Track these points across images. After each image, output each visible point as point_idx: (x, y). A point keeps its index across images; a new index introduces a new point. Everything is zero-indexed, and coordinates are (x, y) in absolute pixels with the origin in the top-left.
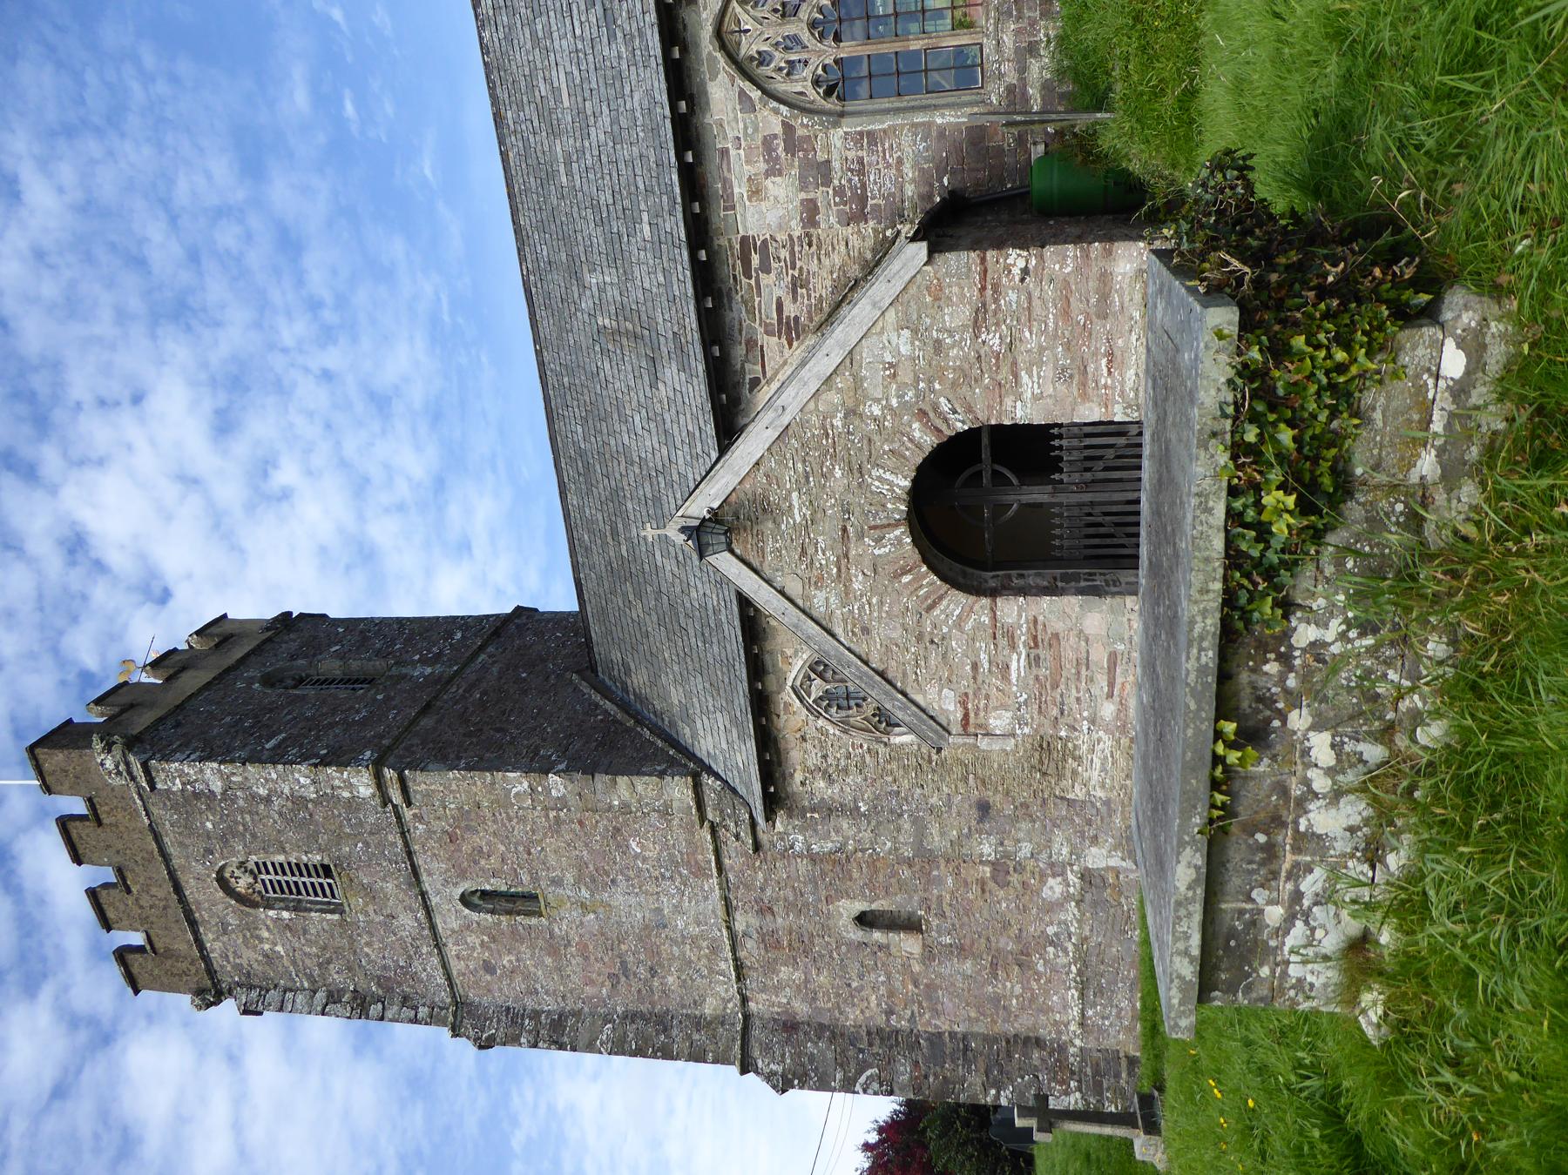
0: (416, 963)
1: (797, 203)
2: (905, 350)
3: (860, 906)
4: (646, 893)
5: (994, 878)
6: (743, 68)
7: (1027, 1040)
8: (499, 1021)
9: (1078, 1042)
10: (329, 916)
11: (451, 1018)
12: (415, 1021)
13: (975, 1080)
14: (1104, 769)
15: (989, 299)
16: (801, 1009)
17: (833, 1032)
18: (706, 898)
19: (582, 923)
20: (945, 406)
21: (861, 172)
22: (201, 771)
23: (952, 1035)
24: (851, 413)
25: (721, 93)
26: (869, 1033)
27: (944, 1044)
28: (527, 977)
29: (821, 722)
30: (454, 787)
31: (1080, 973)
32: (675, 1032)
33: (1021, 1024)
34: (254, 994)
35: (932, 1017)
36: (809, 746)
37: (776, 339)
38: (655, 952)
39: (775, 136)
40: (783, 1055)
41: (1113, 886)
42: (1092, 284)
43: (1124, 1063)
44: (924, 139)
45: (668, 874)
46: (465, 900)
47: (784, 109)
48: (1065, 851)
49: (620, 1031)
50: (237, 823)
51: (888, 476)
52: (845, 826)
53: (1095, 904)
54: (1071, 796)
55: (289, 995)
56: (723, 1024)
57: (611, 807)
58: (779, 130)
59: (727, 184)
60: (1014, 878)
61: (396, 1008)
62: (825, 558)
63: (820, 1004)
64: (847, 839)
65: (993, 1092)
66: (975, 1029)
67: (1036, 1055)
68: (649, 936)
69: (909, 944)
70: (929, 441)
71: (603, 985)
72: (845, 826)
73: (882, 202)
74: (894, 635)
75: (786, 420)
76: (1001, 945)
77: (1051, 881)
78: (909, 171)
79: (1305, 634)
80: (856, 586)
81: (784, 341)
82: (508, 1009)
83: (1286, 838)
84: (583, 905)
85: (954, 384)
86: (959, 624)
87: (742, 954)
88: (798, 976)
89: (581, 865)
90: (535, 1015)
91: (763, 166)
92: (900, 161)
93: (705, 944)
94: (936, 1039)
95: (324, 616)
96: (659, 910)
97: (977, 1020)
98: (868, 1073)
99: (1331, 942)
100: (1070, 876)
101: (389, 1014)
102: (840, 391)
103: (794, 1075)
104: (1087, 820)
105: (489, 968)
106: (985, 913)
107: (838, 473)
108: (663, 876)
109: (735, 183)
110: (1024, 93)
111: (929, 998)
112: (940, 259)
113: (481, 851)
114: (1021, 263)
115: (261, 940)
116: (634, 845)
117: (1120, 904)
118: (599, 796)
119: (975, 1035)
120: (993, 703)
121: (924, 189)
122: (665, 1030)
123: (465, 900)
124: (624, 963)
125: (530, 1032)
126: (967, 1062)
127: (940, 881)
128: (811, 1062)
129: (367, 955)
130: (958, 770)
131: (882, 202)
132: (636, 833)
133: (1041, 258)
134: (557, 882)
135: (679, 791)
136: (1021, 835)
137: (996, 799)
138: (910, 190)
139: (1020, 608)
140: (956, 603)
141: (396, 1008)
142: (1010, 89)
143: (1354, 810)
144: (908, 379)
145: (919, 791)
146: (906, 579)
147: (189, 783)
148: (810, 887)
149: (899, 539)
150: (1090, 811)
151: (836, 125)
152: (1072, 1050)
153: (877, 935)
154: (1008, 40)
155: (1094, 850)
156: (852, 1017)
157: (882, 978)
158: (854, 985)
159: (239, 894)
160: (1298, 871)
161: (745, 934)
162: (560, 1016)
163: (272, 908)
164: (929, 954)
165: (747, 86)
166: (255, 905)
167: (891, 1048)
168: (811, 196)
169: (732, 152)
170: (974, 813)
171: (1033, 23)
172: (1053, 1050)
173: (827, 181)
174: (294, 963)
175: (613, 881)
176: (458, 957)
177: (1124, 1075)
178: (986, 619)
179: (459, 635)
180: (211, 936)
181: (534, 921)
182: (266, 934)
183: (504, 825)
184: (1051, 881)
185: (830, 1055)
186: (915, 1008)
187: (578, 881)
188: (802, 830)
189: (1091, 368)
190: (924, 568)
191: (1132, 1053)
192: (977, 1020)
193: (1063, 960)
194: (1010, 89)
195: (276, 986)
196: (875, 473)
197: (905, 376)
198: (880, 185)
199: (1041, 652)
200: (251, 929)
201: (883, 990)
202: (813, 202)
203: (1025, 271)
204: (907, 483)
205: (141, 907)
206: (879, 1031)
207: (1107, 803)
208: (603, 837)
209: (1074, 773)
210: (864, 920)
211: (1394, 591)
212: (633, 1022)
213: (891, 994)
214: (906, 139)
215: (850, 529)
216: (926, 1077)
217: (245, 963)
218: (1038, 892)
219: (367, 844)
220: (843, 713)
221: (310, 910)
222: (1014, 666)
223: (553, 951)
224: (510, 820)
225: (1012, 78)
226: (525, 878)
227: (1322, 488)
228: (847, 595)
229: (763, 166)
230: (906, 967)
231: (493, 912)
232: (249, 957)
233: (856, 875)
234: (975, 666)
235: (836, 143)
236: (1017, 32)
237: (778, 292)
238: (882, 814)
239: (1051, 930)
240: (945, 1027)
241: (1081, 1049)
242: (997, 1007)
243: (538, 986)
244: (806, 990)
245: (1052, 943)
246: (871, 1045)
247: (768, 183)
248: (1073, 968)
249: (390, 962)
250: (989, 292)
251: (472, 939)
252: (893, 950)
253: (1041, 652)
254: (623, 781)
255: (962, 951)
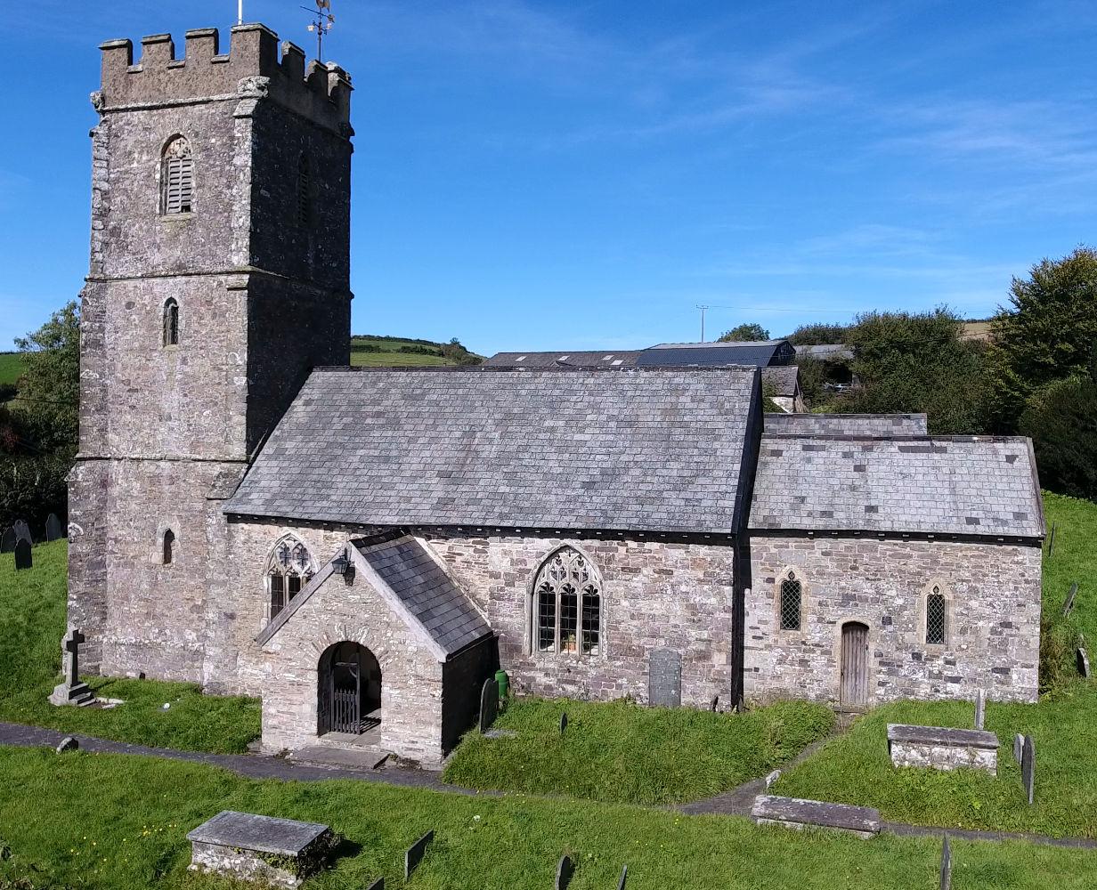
0: (130, 257)
3: (177, 534)
5: (195, 605)
6: (555, 554)
7: (105, 613)
8: (97, 307)
9: (105, 640)
10: (158, 206)
12: (93, 252)
13: (81, 587)
14: (252, 674)
16: (115, 491)
17: (102, 508)
18: (178, 448)
20: (389, 661)
21: (509, 600)
23: (105, 574)
25: (546, 545)
26: (103, 528)
27: (99, 569)
28: (126, 328)
30: (238, 319)
31: (145, 645)
32: (97, 416)
33: (112, 609)
34: (104, 139)
36: (262, 535)
37: (447, 550)
38: (145, 410)
40: (87, 481)
41: (193, 666)
42: (428, 720)
43: (96, 664)
44: (519, 628)
46: (171, 300)
47: (536, 570)
48: (211, 653)
49: (95, 383)
50: (215, 160)
51: (364, 636)
53: (183, 656)
55: (105, 164)
57: (229, 410)
58: (528, 567)
60: (195, 616)
61: (101, 238)
62: (335, 605)
63: (119, 502)
64: (214, 546)
65: (75, 597)
66: (109, 586)
67: (97, 618)
69: (157, 557)
70: (376, 653)
71: (123, 375)
73: (497, 607)
77: (194, 635)
78: (507, 619)
79: (255, 860)
82: (105, 312)
84: (171, 374)
86: (307, 655)
88: (135, 493)
89: (195, 378)
90: (102, 329)
91: (515, 558)
92: (512, 617)
93: (151, 441)
94: (102, 564)
95: (353, 152)
96: (170, 418)
98: (81, 529)
99: (205, 861)
101: (97, 234)
102: (397, 621)
103: (77, 488)
104: (228, 662)
105: (130, 305)
107: (366, 616)
108: (190, 425)
110: (530, 670)
111: (126, 563)
112: (440, 666)
113: (201, 318)
115: (141, 153)
116: (208, 412)
118: (234, 405)
119: (106, 586)
120: (275, 665)
122: (97, 410)
123: (171, 300)
124: (137, 390)
125: (91, 327)
126: (90, 583)
127: (192, 577)
129: (134, 225)
130: (250, 607)
131: (497, 607)
133: (438, 701)
134: (184, 361)
135: (239, 450)
137: (236, 623)
138: (501, 619)
140: (316, 656)
141: (101, 238)
142: (534, 665)
143: (228, 866)
145: (240, 586)
146: (325, 636)
147: (239, 143)
151: (528, 592)
152: (101, 637)
153: (161, 540)
154: (552, 665)
155: (212, 667)
156: (112, 519)
157: (136, 540)
158: (131, 523)
161: (158, 466)
164: (151, 567)
165: (546, 557)
166: (163, 153)
169: (522, 545)
170: (229, 612)
171: (556, 676)
173: (507, 585)
174: (126, 172)
175: (185, 395)
176: (136, 287)
177: (90, 664)
179: (334, 265)
180: (142, 117)
181: (161, 341)
182: (145, 158)
184: (194, 635)
185: (89, 507)
188: (219, 524)
190: (329, 645)
192: (115, 588)
193: (151, 637)
194: (534, 665)
195: (109, 154)
197: (400, 647)
200: (148, 149)
201: (129, 539)
203: (434, 696)
205: (159, 74)
207: (236, 675)
209: (250, 661)
210: (169, 536)
211: (263, 873)
213: (127, 543)
219: (203, 245)
220: (278, 555)
221: (161, 193)
222: (290, 675)
223: (143, 349)
225: (538, 666)
226: (187, 342)
227: (275, 864)
228: (319, 612)
229: (515, 558)
230: (144, 554)
231: (165, 316)
232: (129, 141)
234: (290, 659)
235: (521, 590)
236: (554, 670)
238: (227, 565)
239: (168, 632)
240: (109, 570)
241: (102, 642)
243: (119, 334)
244: (126, 496)
245: (160, 631)
246: (97, 530)
247: (508, 559)
248: (147, 642)
249: (129, 240)
252: (152, 548)
254: (243, 419)
255: (154, 585)
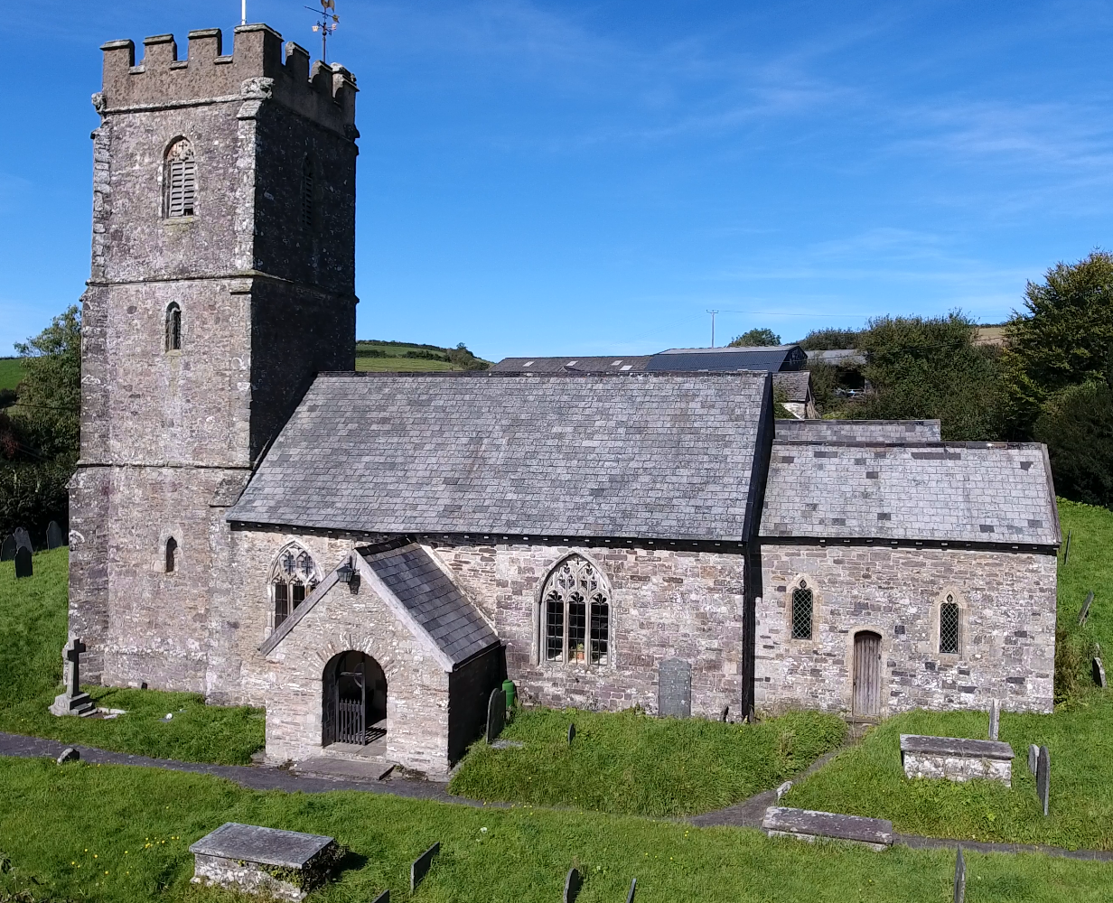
0: (132, 261)
1: (507, 579)
2: (416, 658)
3: (180, 541)
4: (182, 420)
5: (198, 614)
6: (563, 562)
7: (107, 622)
8: (98, 311)
9: (107, 649)
10: (160, 209)
11: (98, 281)
12: (95, 256)
13: (82, 596)
14: (255, 684)
15: (432, 692)
16: (116, 498)
18: (181, 455)
19: (163, 376)
21: (516, 608)
22: (250, 156)
23: (107, 582)
24: (394, 633)
25: (554, 553)
26: (104, 536)
27: (101, 577)
29: (277, 552)
30: (242, 324)
31: (147, 654)
32: (98, 422)
33: (114, 618)
34: (106, 141)
35: (116, 572)
36: (265, 543)
38: (147, 416)
39: (533, 573)
41: (196, 676)
42: (434, 730)
45: (194, 434)
46: (174, 305)
47: (544, 579)
48: (214, 662)
50: (218, 162)
52: (224, 554)
54: (242, 668)
55: (107, 166)
56: (105, 451)
57: (232, 416)
58: (536, 575)
59: (517, 549)
60: (198, 625)
61: (102, 241)
63: (120, 509)
64: (218, 554)
65: (76, 606)
66: (111, 595)
68: (156, 415)
69: (160, 565)
70: (382, 663)
72: (224, 554)
74: (307, 638)
75: (392, 608)
76: (160, 614)
77: (197, 644)
78: (514, 629)
79: (259, 873)
80: (327, 625)
81: (453, 562)
82: (106, 317)
83: (226, 868)
84: (173, 379)
85: (402, 675)
86: (311, 665)
87: (148, 469)
88: (137, 500)
90: (103, 334)
91: (522, 566)
92: (519, 626)
93: (153, 448)
94: (103, 573)
95: (358, 154)
97: (116, 596)
98: (82, 537)
99: (208, 874)
100: (200, 654)
103: (78, 495)
104: (232, 672)
105: (131, 310)
106: (179, 608)
107: (372, 625)
108: (193, 431)
109: (517, 552)
111: (127, 572)
112: (447, 676)
113: (204, 323)
114: (443, 705)
115: (143, 155)
116: (211, 418)
117: (186, 678)
119: (107, 594)
120: (279, 675)
121: (507, 635)
124: (139, 396)
126: (92, 591)
127: (195, 586)
128: (86, 504)
129: (136, 228)
132: (217, 420)
133: (445, 712)
134: (187, 366)
135: (242, 457)
136: (222, 642)
137: (240, 632)
138: (508, 628)
139: (318, 690)
141: (102, 241)
142: (542, 674)
143: (231, 879)
144: (405, 658)
145: (243, 595)
146: (330, 646)
148: (189, 515)
149: (345, 646)
150: (235, 676)
151: (535, 600)
152: (102, 646)
153: (163, 548)
154: (560, 675)
155: (215, 677)
156: (113, 526)
157: (138, 547)
158: (133, 531)
159: (172, 146)
160: (221, 870)
161: (160, 473)
162: (104, 350)
163: (164, 170)
164: (153, 575)
165: (554, 564)
166: (166, 155)
167: (97, 549)
168: (509, 585)
170: (233, 621)
171: (565, 685)
172: (101, 636)
173: (514, 593)
174: (128, 175)
175: (188, 401)
176: (138, 291)
177: (91, 674)
178: (313, 676)
180: (144, 119)
181: (163, 346)
183: (221, 342)
184: (197, 644)
185: (91, 515)
186: (121, 563)
187: (188, 379)
188: (222, 531)
189: (405, 726)
190: (334, 654)
191: (102, 677)
192: (116, 596)
194: (542, 674)
196: (371, 640)
197: (406, 657)
198: (511, 616)
199: (300, 696)
200: (150, 151)
201: (131, 546)
202: (507, 586)
203: (440, 706)
204: (367, 652)
206: (107, 542)
207: (239, 685)
208: (214, 400)
209: (254, 671)
210: (171, 544)
211: (266, 886)
212: (103, 396)
213: (129, 551)
214: (527, 629)
215: (350, 626)
216: (82, 569)
217: (126, 138)
218: (191, 637)
219: (206, 249)
220: (282, 563)
221: (164, 196)
222: (294, 685)
223: (145, 354)
224: (224, 346)
225: (546, 676)
226: (190, 347)
227: (279, 877)
228: (324, 621)
229: (522, 566)
230: (146, 562)
231: (167, 321)
232: (131, 143)
233: (197, 541)
234: (294, 669)
235: (528, 598)
236: (562, 680)
237: (473, 562)
239: (170, 641)
240: (111, 578)
241: (103, 651)
242: (124, 607)
243: (121, 339)
244: (127, 503)
245: (163, 641)
246: (98, 537)
248: (149, 651)
250: (434, 692)
251: (149, 304)
252: (154, 556)
253: (300, 696)
254: (247, 426)
255: (157, 593)
